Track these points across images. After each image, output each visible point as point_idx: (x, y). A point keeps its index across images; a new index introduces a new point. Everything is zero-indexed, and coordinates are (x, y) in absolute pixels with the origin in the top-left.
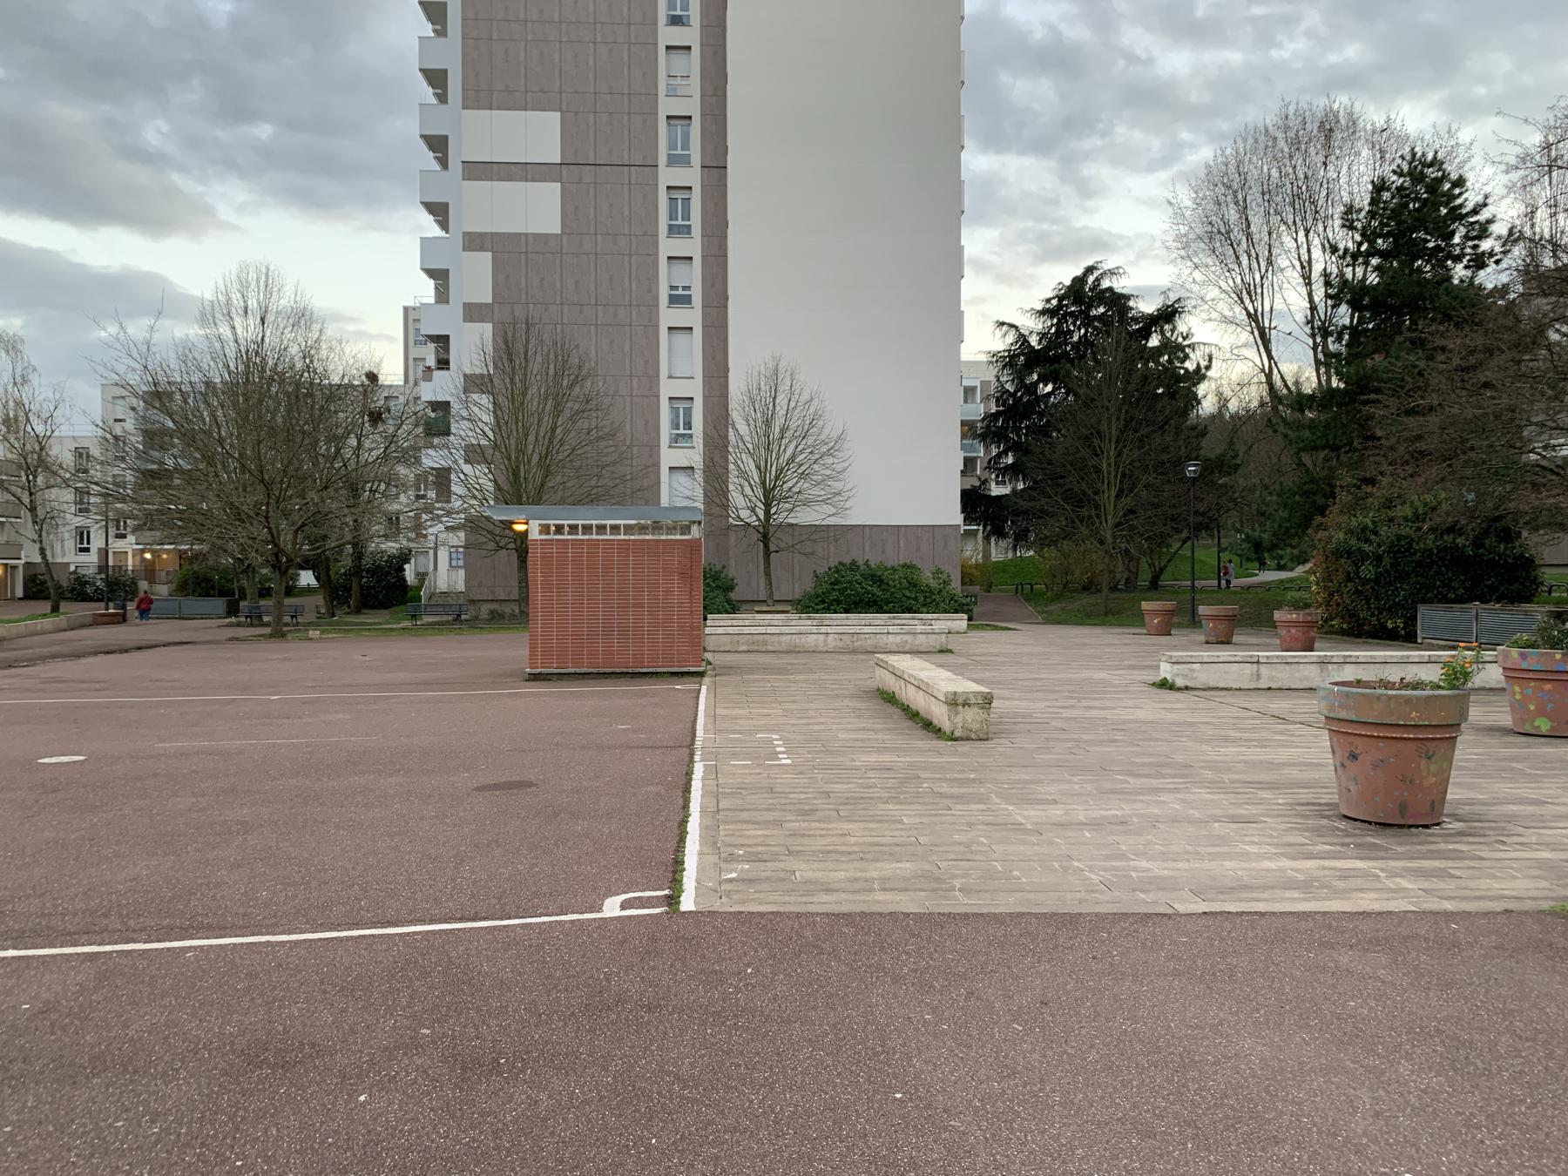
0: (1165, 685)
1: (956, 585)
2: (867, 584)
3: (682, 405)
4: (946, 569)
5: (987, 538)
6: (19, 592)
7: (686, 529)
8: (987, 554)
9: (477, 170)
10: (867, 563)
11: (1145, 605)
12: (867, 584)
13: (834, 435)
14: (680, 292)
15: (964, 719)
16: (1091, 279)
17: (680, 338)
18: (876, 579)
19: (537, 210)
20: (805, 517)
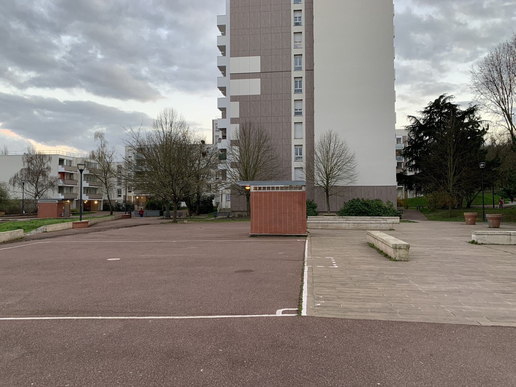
0: (473, 242)
1: (395, 207)
2: (363, 206)
3: (299, 148)
4: (392, 201)
5: (406, 190)
6: (102, 209)
7: (301, 188)
8: (406, 196)
9: (235, 76)
10: (363, 199)
11: (465, 214)
12: (363, 206)
13: (351, 156)
14: (298, 111)
15: (400, 254)
16: (442, 100)
17: (298, 126)
18: (366, 204)
19: (253, 88)
20: (341, 183)
